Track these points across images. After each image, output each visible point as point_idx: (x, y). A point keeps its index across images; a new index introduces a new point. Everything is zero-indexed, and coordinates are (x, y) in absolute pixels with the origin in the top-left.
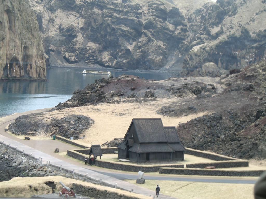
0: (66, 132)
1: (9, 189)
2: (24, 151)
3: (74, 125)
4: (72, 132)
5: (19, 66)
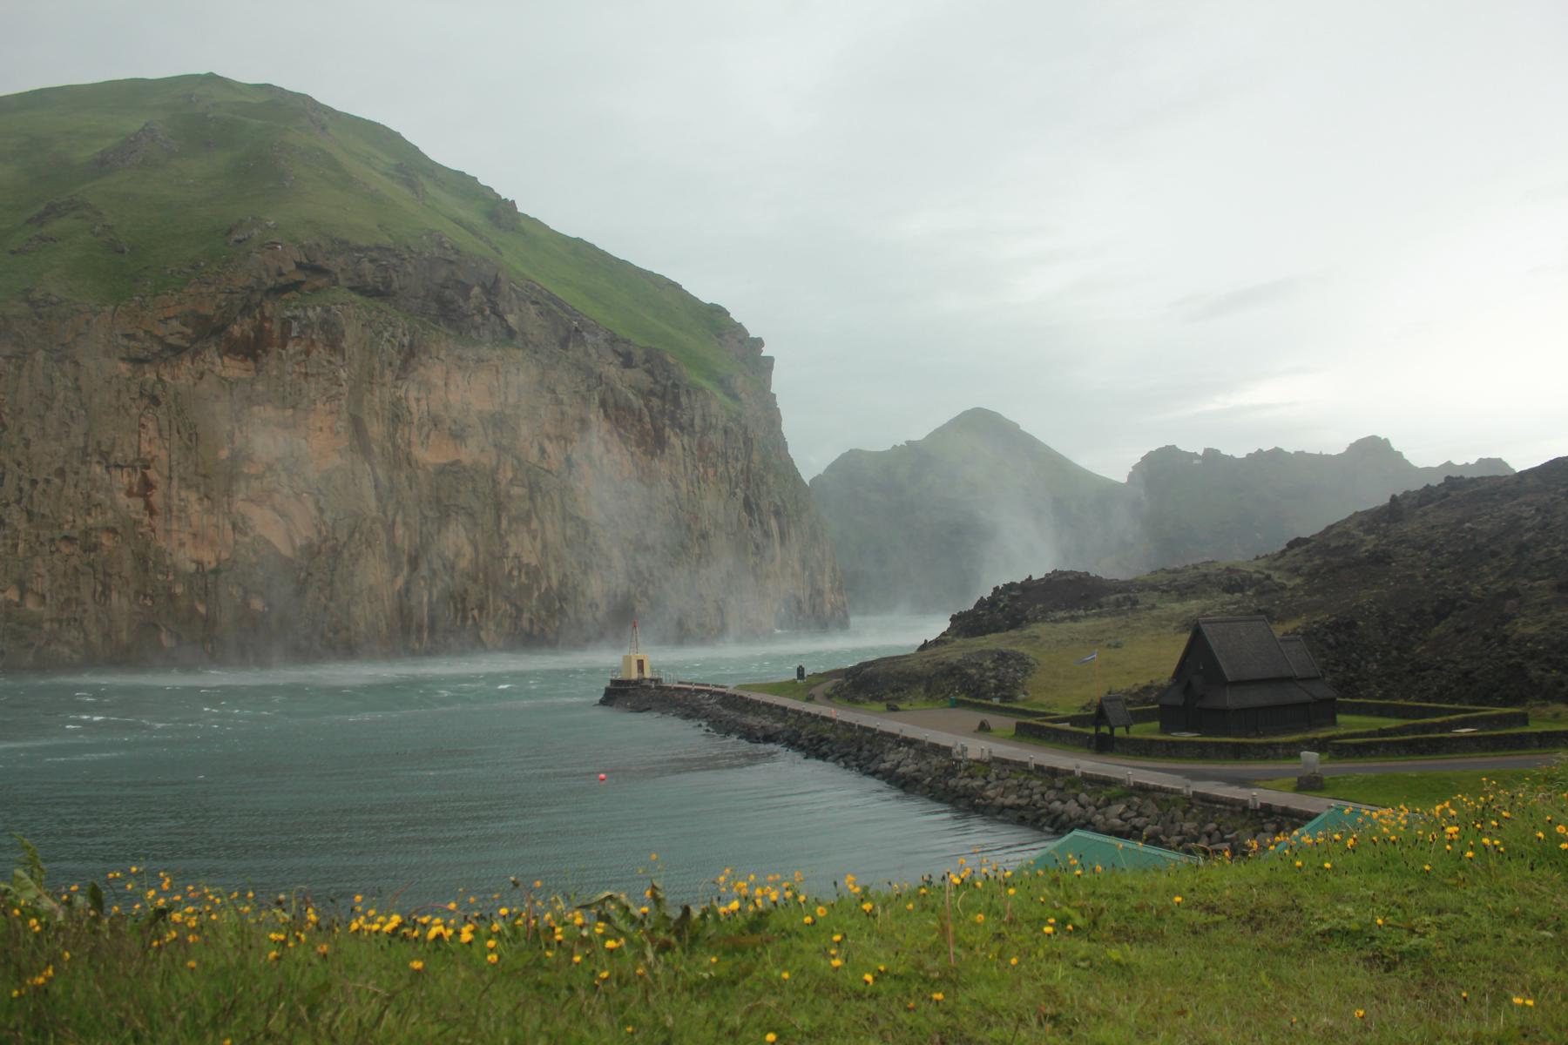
0: (979, 687)
1: (683, 719)
2: (901, 731)
3: (994, 669)
4: (992, 685)
5: (797, 933)
